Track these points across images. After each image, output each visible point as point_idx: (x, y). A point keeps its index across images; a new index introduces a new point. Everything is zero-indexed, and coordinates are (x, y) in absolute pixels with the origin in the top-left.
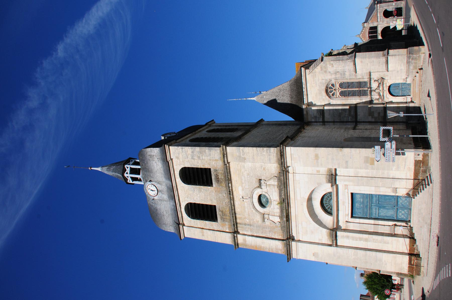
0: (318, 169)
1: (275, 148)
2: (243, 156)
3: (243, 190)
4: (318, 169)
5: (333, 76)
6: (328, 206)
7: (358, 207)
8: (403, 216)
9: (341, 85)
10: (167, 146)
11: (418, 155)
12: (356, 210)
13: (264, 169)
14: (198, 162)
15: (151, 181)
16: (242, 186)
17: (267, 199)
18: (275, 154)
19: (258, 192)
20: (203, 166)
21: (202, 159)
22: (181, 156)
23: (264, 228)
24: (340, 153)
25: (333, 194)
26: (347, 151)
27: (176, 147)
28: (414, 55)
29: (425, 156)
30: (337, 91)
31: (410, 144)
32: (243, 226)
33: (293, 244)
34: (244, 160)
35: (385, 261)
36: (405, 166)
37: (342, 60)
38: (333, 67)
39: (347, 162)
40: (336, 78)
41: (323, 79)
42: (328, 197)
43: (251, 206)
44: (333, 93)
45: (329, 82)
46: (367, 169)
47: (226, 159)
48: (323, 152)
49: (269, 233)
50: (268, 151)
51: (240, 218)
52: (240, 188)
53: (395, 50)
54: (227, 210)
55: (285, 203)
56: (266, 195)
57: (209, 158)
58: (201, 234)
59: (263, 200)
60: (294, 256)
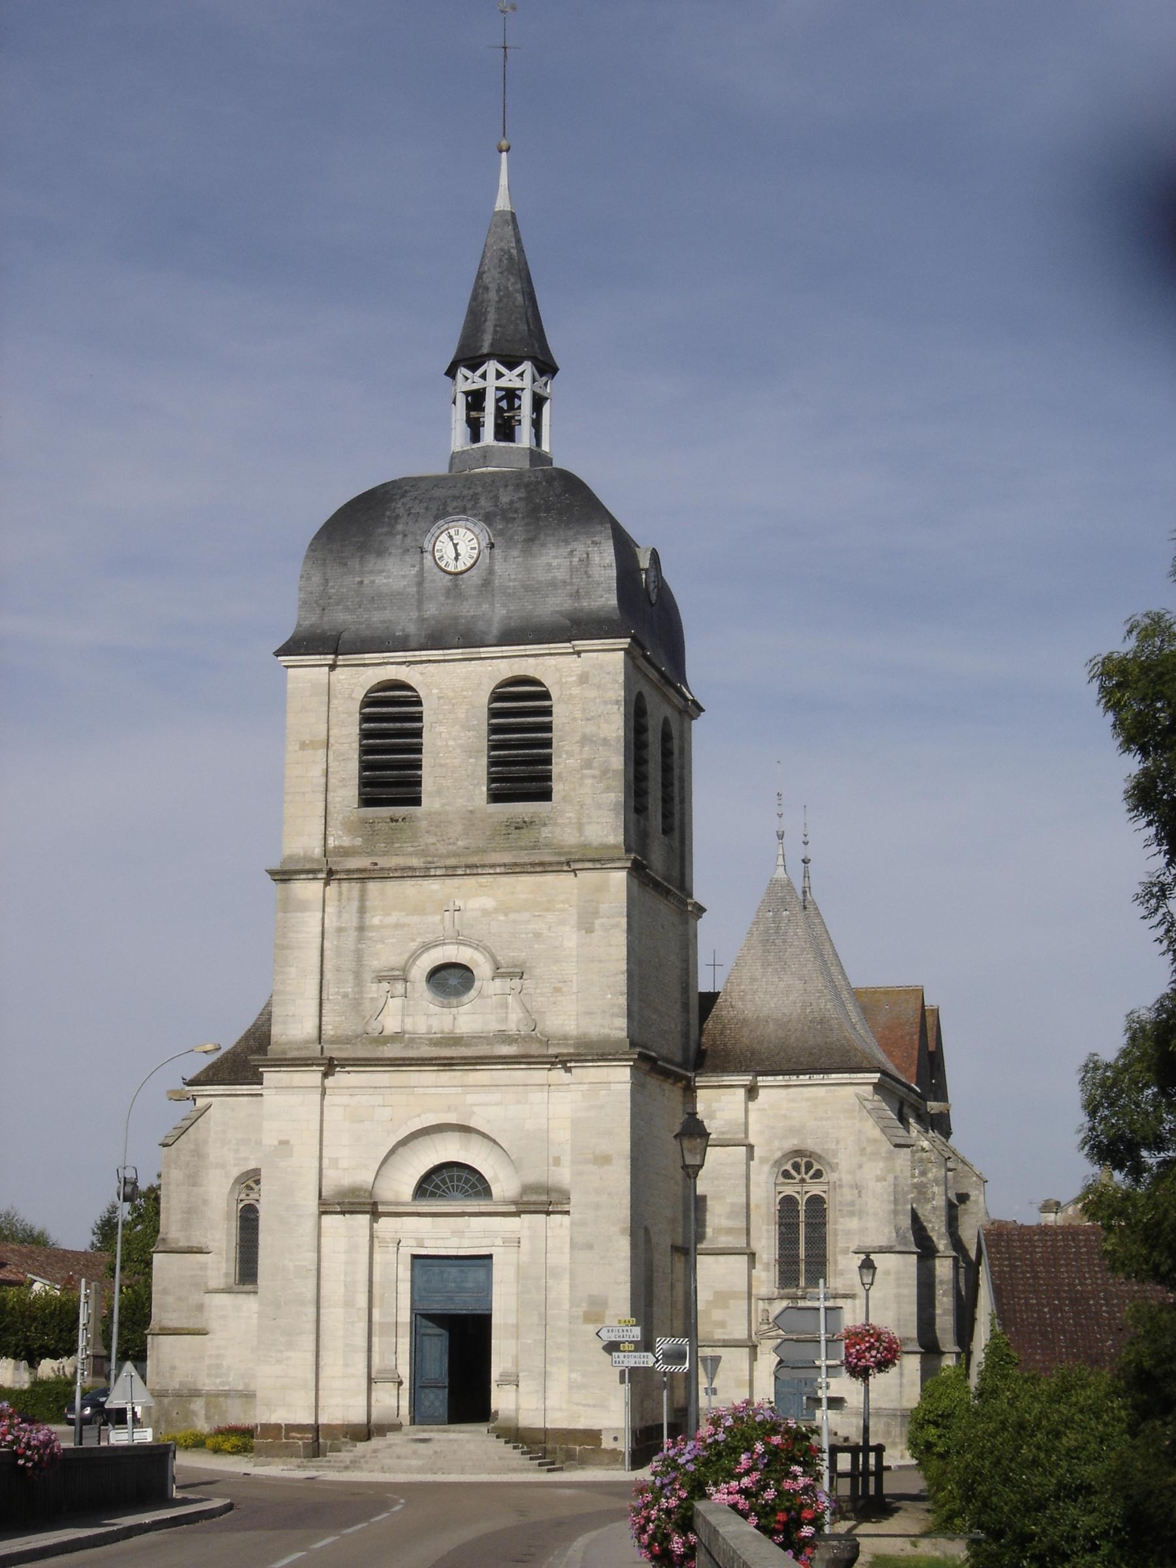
0: (566, 1159)
1: (625, 1034)
3: (485, 912)
4: (566, 1159)
5: (847, 1179)
6: (444, 1183)
7: (445, 1275)
8: (427, 1403)
9: (816, 1203)
10: (625, 642)
11: (616, 1439)
12: (436, 1270)
13: (557, 990)
14: (570, 755)
15: (492, 546)
16: (496, 910)
18: (606, 1031)
19: (482, 968)
21: (583, 777)
22: (593, 693)
26: (623, 1246)
27: (621, 678)
28: (898, 1429)
29: (614, 1455)
30: (798, 1189)
31: (642, 1418)
32: (355, 904)
33: (313, 1077)
34: (586, 926)
35: (289, 1358)
36: (584, 1405)
37: (895, 1212)
39: (590, 1247)
40: (841, 1186)
41: (838, 1143)
42: (467, 1181)
43: (429, 938)
44: (793, 1173)
45: (829, 1163)
46: (573, 1303)
48: (618, 1178)
49: (337, 993)
50: (616, 1010)
52: (488, 902)
53: (919, 1373)
55: (453, 1057)
56: (473, 993)
57: (588, 801)
59: (453, 979)
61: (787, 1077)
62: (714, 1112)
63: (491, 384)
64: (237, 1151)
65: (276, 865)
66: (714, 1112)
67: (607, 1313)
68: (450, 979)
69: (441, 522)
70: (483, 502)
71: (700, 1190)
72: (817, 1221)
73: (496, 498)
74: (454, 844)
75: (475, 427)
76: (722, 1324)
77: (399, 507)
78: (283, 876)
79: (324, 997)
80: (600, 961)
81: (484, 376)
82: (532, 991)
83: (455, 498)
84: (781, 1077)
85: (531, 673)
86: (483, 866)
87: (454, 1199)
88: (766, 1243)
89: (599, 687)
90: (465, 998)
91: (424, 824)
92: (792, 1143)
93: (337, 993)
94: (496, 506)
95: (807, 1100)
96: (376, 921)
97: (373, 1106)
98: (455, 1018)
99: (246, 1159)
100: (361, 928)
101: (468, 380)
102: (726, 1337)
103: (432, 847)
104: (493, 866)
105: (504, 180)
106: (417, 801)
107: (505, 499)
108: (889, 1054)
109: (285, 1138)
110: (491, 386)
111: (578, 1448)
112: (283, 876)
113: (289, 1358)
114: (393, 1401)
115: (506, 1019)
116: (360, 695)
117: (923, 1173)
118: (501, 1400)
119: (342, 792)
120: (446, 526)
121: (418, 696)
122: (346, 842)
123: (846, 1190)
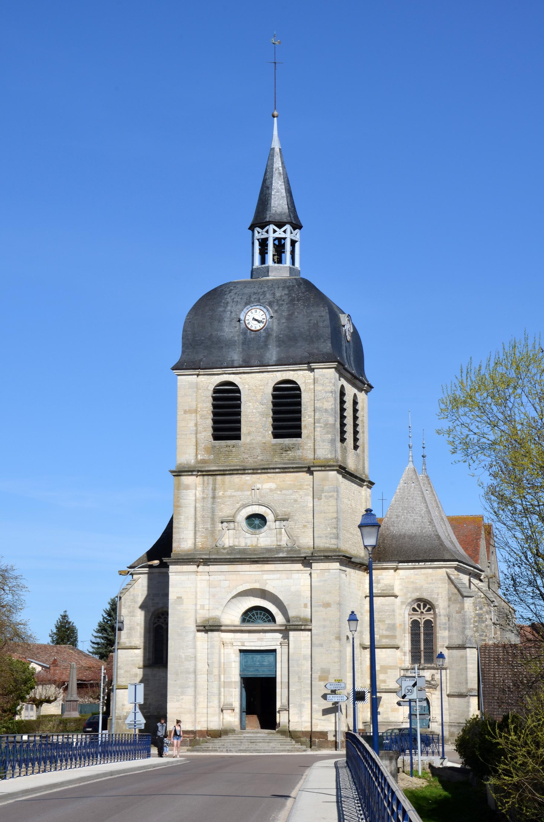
2: (323, 497)
3: (271, 490)
6: (257, 614)
7: (255, 659)
12: (251, 656)
13: (305, 526)
16: (276, 489)
17: (260, 527)
18: (328, 545)
19: (270, 517)
20: (305, 426)
23: (213, 519)
24: (334, 637)
25: (273, 624)
30: (419, 617)
32: (211, 486)
35: (183, 699)
36: (320, 720)
38: (457, 613)
40: (440, 615)
41: (438, 595)
47: (318, 469)
49: (203, 528)
51: (223, 482)
52: (273, 486)
54: (234, 462)
56: (266, 527)
58: (187, 408)
59: (257, 522)
60: (290, 632)
61: (414, 564)
62: (379, 580)
63: (271, 236)
64: (153, 599)
65: (174, 469)
66: (379, 580)
67: (330, 676)
68: (257, 521)
69: (249, 306)
70: (268, 296)
71: (345, 422)
72: (429, 632)
73: (274, 294)
74: (256, 458)
75: (263, 261)
76: (384, 681)
77: (228, 298)
78: (178, 473)
79: (197, 529)
80: (325, 513)
81: (267, 232)
82: (293, 527)
83: (255, 293)
84: (410, 564)
85: (291, 378)
86: (270, 469)
87: (259, 623)
88: (406, 643)
89: (323, 385)
90: (262, 530)
91: (242, 449)
92: (417, 595)
93: (203, 528)
94: (274, 298)
95: (424, 574)
96: (221, 494)
97: (221, 580)
98: (258, 539)
99: (158, 603)
100: (214, 498)
101: (259, 234)
102: (386, 688)
103: (246, 460)
104: (273, 469)
105: (275, 132)
106: (238, 438)
107: (278, 294)
108: (466, 550)
109: (180, 596)
110: (271, 236)
111: (317, 740)
112: (178, 473)
113: (183, 699)
114: (232, 719)
115: (281, 540)
116: (211, 388)
117: (481, 609)
118: (281, 718)
119: (204, 434)
120: (251, 308)
121: (239, 389)
122: (206, 457)
123: (442, 617)
